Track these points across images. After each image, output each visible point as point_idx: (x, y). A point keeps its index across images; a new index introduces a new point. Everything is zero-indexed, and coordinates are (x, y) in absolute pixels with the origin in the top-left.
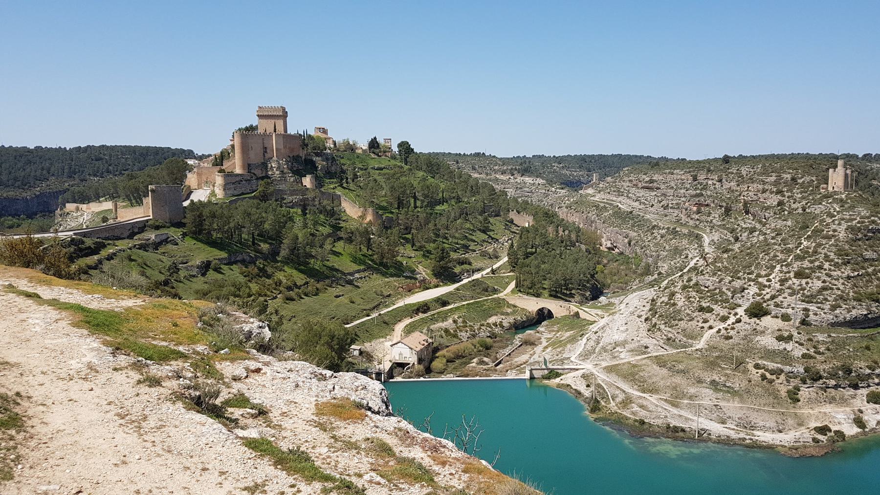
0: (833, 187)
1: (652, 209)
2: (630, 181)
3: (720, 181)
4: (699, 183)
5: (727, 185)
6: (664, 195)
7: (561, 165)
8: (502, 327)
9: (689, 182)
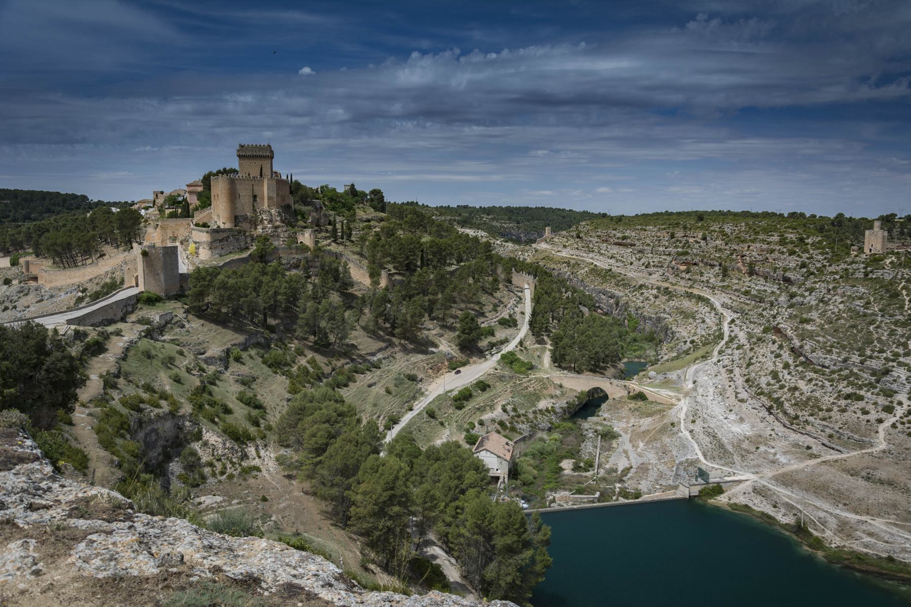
0: (871, 250)
1: (632, 267)
2: (599, 236)
3: (704, 239)
4: (677, 241)
5: (714, 244)
6: (640, 251)
7: (490, 217)
8: (555, 413)
9: (666, 239)
